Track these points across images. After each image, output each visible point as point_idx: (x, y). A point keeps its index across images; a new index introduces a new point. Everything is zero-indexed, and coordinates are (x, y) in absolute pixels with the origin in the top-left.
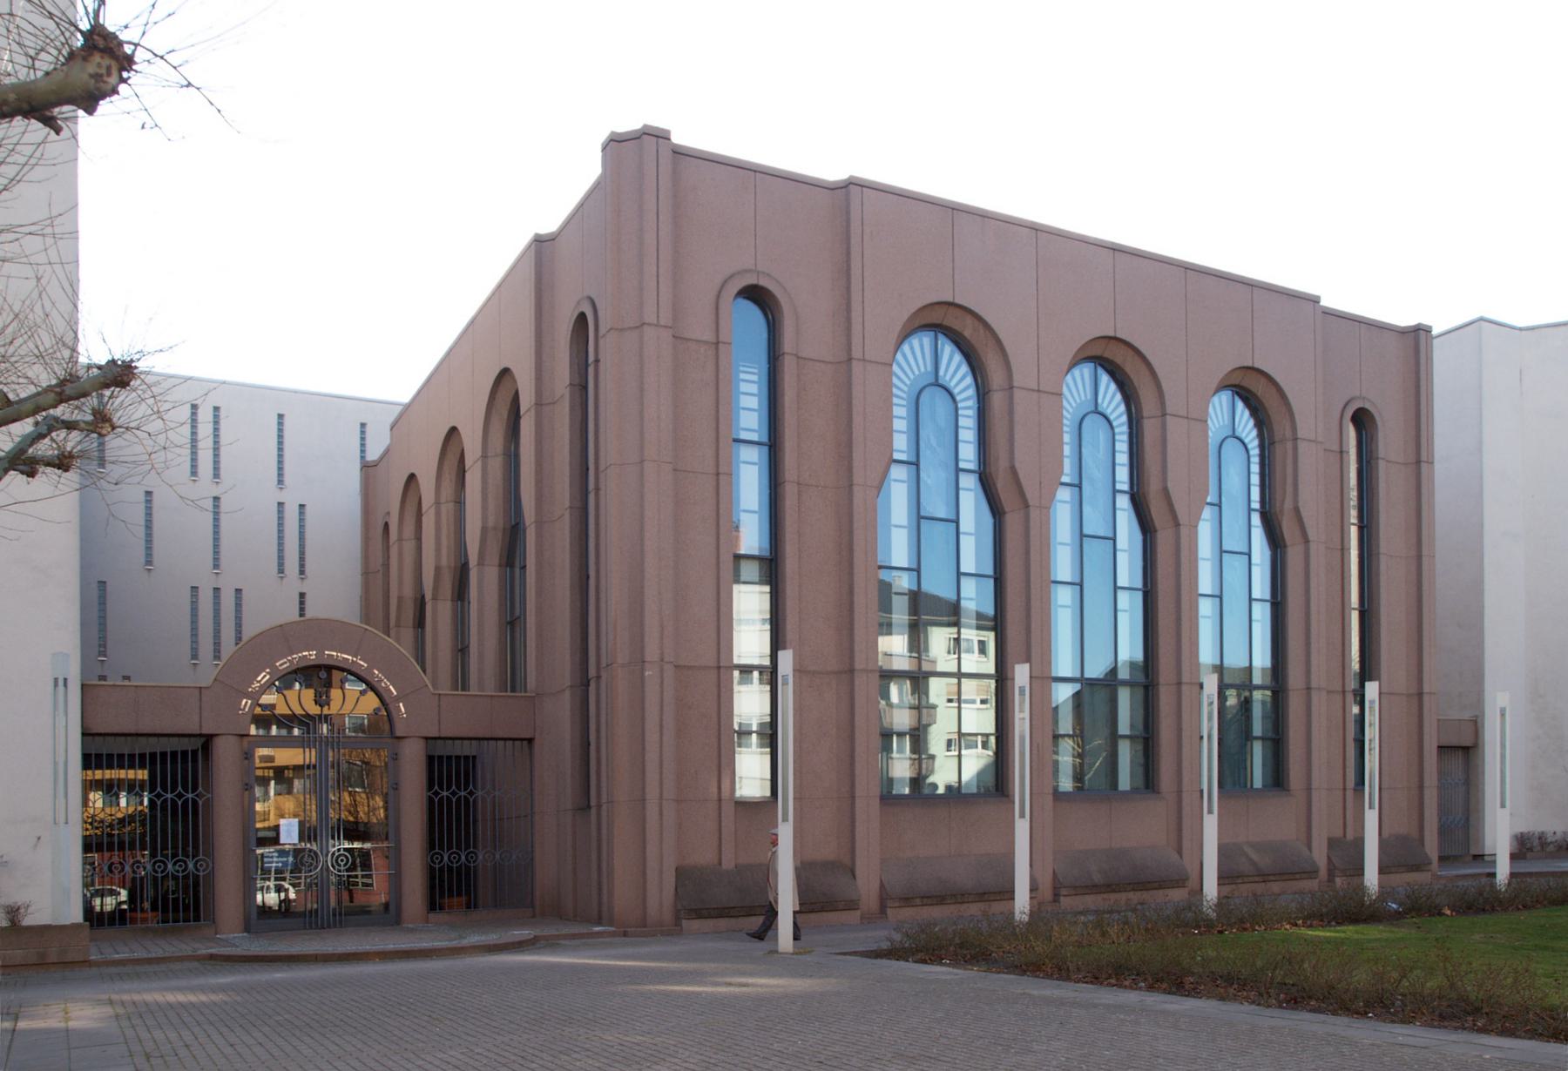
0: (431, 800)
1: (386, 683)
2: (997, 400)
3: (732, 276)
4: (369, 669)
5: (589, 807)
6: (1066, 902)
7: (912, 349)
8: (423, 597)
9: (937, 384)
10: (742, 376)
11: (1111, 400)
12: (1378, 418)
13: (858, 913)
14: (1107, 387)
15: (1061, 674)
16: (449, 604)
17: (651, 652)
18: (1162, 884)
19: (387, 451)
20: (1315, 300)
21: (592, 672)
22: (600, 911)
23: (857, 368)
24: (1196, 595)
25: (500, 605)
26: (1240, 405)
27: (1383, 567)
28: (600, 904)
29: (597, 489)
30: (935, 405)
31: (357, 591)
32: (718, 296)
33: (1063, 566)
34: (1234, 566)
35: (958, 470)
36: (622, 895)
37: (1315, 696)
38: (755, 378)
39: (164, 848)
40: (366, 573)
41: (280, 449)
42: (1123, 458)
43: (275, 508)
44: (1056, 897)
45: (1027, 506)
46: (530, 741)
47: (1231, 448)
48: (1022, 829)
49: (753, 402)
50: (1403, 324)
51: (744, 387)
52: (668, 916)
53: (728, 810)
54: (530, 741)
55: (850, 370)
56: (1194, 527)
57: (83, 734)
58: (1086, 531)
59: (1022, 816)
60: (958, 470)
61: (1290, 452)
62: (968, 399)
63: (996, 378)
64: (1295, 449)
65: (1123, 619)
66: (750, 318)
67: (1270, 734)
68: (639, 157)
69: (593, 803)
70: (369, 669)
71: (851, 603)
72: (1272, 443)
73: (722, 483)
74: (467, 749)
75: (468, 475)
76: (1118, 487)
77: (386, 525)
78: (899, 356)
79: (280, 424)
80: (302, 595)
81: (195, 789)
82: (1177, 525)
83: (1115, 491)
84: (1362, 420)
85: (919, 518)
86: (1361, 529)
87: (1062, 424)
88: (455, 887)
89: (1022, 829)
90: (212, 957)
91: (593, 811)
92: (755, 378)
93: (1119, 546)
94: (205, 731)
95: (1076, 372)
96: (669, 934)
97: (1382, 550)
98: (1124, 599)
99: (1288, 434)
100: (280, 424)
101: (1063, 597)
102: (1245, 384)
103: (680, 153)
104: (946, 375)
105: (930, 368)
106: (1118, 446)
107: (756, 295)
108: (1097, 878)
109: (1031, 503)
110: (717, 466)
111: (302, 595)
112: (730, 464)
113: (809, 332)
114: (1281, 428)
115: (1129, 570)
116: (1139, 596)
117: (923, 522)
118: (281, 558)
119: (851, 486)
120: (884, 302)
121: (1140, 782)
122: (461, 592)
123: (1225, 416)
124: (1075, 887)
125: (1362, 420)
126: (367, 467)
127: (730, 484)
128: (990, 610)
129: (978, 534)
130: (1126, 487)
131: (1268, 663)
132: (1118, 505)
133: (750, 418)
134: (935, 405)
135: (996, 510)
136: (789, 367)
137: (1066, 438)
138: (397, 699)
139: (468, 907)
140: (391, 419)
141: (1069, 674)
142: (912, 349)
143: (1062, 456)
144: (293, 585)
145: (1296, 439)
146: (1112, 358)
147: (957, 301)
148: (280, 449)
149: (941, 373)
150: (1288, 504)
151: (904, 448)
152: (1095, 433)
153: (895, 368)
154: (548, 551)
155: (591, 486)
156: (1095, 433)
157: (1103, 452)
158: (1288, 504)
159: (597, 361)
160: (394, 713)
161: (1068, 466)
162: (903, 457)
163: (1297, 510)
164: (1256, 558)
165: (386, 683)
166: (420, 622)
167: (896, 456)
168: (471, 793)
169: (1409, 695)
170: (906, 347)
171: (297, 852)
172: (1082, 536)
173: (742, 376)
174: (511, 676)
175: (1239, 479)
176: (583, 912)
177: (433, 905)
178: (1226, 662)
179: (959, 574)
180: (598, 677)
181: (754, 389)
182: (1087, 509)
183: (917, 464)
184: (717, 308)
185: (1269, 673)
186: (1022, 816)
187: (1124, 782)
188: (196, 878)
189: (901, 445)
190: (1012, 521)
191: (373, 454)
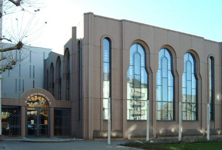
0: (55, 118)
1: (48, 99)
2: (147, 55)
3: (103, 36)
4: (45, 97)
5: (80, 120)
6: (159, 138)
7: (132, 48)
8: (54, 83)
9: (137, 52)
10: (105, 51)
11: (141, 50)
12: (214, 58)
13: (123, 139)
14: (167, 53)
16: (58, 85)
17: (90, 96)
18: (175, 136)
19: (48, 58)
20: (203, 38)
21: (81, 98)
22: (81, 137)
23: (123, 50)
24: (182, 88)
27: (215, 83)
28: (81, 136)
29: (81, 69)
30: (137, 56)
31: (43, 75)
34: (189, 83)
35: (141, 67)
36: (85, 135)
37: (203, 105)
39: (15, 133)
40: (45, 78)
41: (34, 84)
43: (33, 82)
44: (157, 137)
45: (152, 73)
46: (71, 109)
49: (107, 56)
51: (105, 53)
52: (92, 138)
53: (102, 121)
54: (71, 109)
55: (122, 51)
56: (181, 76)
57: (2, 105)
61: (199, 64)
62: (143, 55)
63: (147, 52)
64: (199, 63)
65: (169, 91)
66: (106, 43)
68: (90, 18)
69: (81, 119)
70: (45, 97)
71: (122, 76)
72: (196, 62)
73: (101, 69)
74: (60, 109)
75: (61, 64)
76: (169, 69)
77: (48, 70)
78: (131, 48)
79: (34, 82)
80: (34, 81)
81: (18, 114)
82: (178, 76)
83: (168, 70)
84: (212, 58)
86: (212, 91)
87: (158, 59)
88: (58, 133)
90: (22, 141)
91: (81, 121)
94: (20, 105)
95: (161, 50)
96: (92, 141)
97: (215, 64)
98: (169, 88)
99: (198, 61)
100: (34, 82)
103: (95, 16)
104: (139, 51)
105: (136, 50)
106: (168, 63)
107: (108, 39)
109: (153, 72)
111: (34, 81)
112: (103, 66)
113: (116, 45)
114: (197, 60)
115: (170, 83)
116: (172, 88)
117: (135, 69)
118: (30, 75)
119: (122, 70)
120: (129, 37)
122: (60, 83)
124: (160, 136)
125: (212, 58)
126: (45, 60)
127: (103, 69)
128: (146, 83)
129: (144, 77)
130: (193, 73)
131: (195, 94)
132: (168, 72)
133: (106, 58)
134: (137, 56)
135: (148, 73)
136: (112, 50)
137: (159, 61)
138: (50, 101)
139: (61, 135)
140: (49, 53)
141: (160, 100)
142: (133, 47)
144: (32, 79)
145: (199, 62)
146: (169, 48)
147: (141, 39)
148: (34, 84)
149: (138, 50)
150: (198, 72)
151: (132, 63)
152: (164, 60)
153: (130, 50)
154: (73, 77)
155: (81, 68)
156: (164, 60)
157: (166, 64)
158: (198, 72)
159: (81, 48)
160: (49, 104)
161: (160, 66)
162: (132, 65)
163: (200, 73)
164: (169, 79)
165: (48, 99)
166: (53, 87)
167: (130, 64)
168: (61, 117)
169: (220, 105)
170: (132, 47)
171: (33, 125)
174: (68, 98)
175: (190, 68)
176: (79, 135)
177: (55, 135)
178: (187, 94)
180: (82, 99)
181: (107, 53)
182: (163, 73)
183: (134, 66)
185: (195, 96)
188: (18, 128)
189: (131, 62)
190: (150, 75)
191: (46, 58)
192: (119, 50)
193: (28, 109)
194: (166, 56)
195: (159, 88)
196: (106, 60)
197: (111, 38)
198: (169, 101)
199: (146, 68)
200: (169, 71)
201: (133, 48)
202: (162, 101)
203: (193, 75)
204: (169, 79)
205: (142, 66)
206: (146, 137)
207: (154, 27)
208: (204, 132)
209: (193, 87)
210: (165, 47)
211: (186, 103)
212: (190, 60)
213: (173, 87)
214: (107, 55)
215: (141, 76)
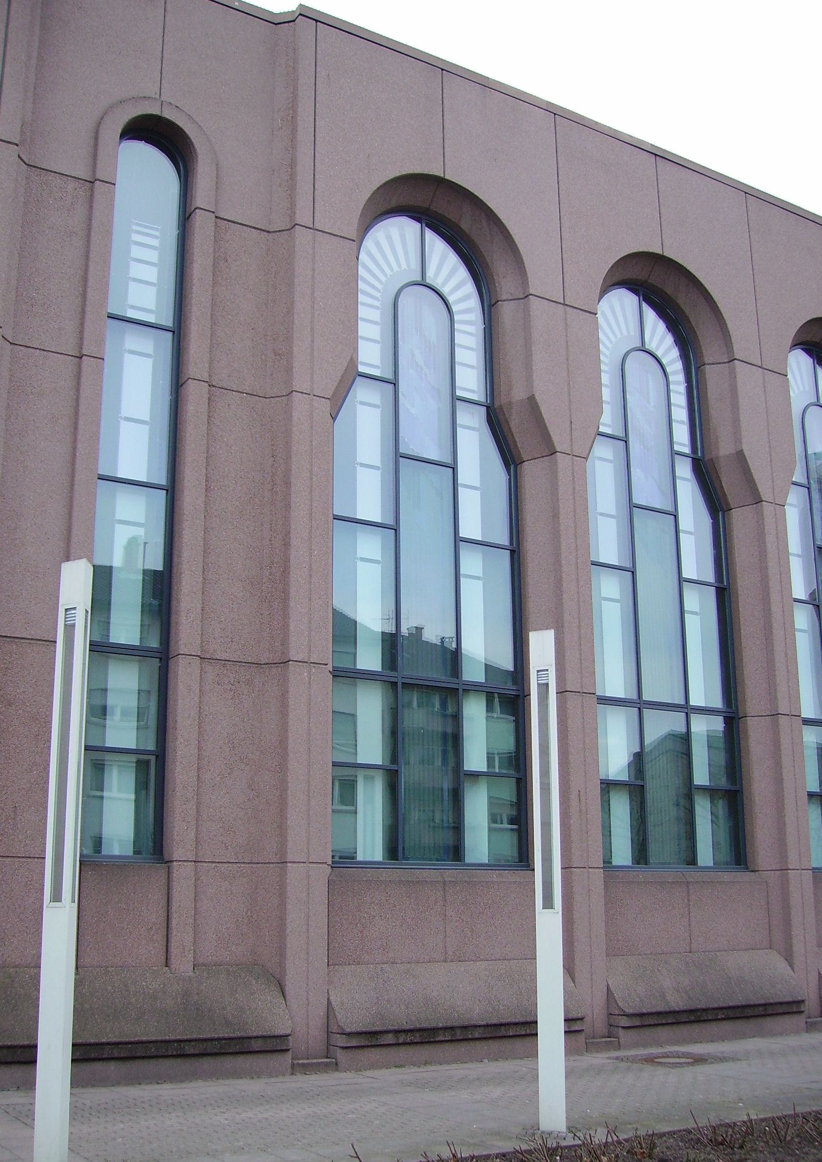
10: (135, 237)
11: (447, 267)
15: (609, 693)
25: (175, 587)
26: (650, 315)
32: (99, 124)
33: (607, 544)
34: (650, 530)
38: (155, 243)
42: (680, 414)
47: (637, 366)
48: (549, 927)
50: (276, 10)
58: (636, 500)
59: (548, 903)
60: (455, 399)
62: (465, 298)
67: (723, 782)
76: (676, 448)
85: (398, 457)
89: (549, 927)
92: (155, 243)
93: (682, 526)
101: (609, 588)
102: (654, 280)
107: (156, 131)
108: (676, 1001)
110: (81, 346)
116: (711, 594)
121: (725, 854)
123: (621, 317)
127: (99, 373)
129: (484, 489)
130: (687, 450)
132: (678, 473)
135: (511, 458)
143: (599, 401)
146: (658, 282)
164: (686, 520)
167: (602, 429)
172: (632, 506)
173: (135, 237)
179: (681, 580)
182: (636, 473)
184: (96, 138)
186: (548, 903)
187: (705, 855)
192: (706, 360)
193: (623, 854)
194: (651, 345)
195: (609, 588)
196: (133, 307)
197: (180, 123)
198: (692, 702)
199: (496, 422)
200: (678, 460)
201: (396, 245)
202: (639, 705)
203: (684, 470)
204: (463, 477)
205: (676, 448)
206: (33, 1062)
207: (555, 113)
208: (600, 998)
209: (689, 572)
210: (635, 272)
211: (639, 705)
212: (647, 346)
213: (512, 552)
214: (155, 270)
215: (461, 480)
